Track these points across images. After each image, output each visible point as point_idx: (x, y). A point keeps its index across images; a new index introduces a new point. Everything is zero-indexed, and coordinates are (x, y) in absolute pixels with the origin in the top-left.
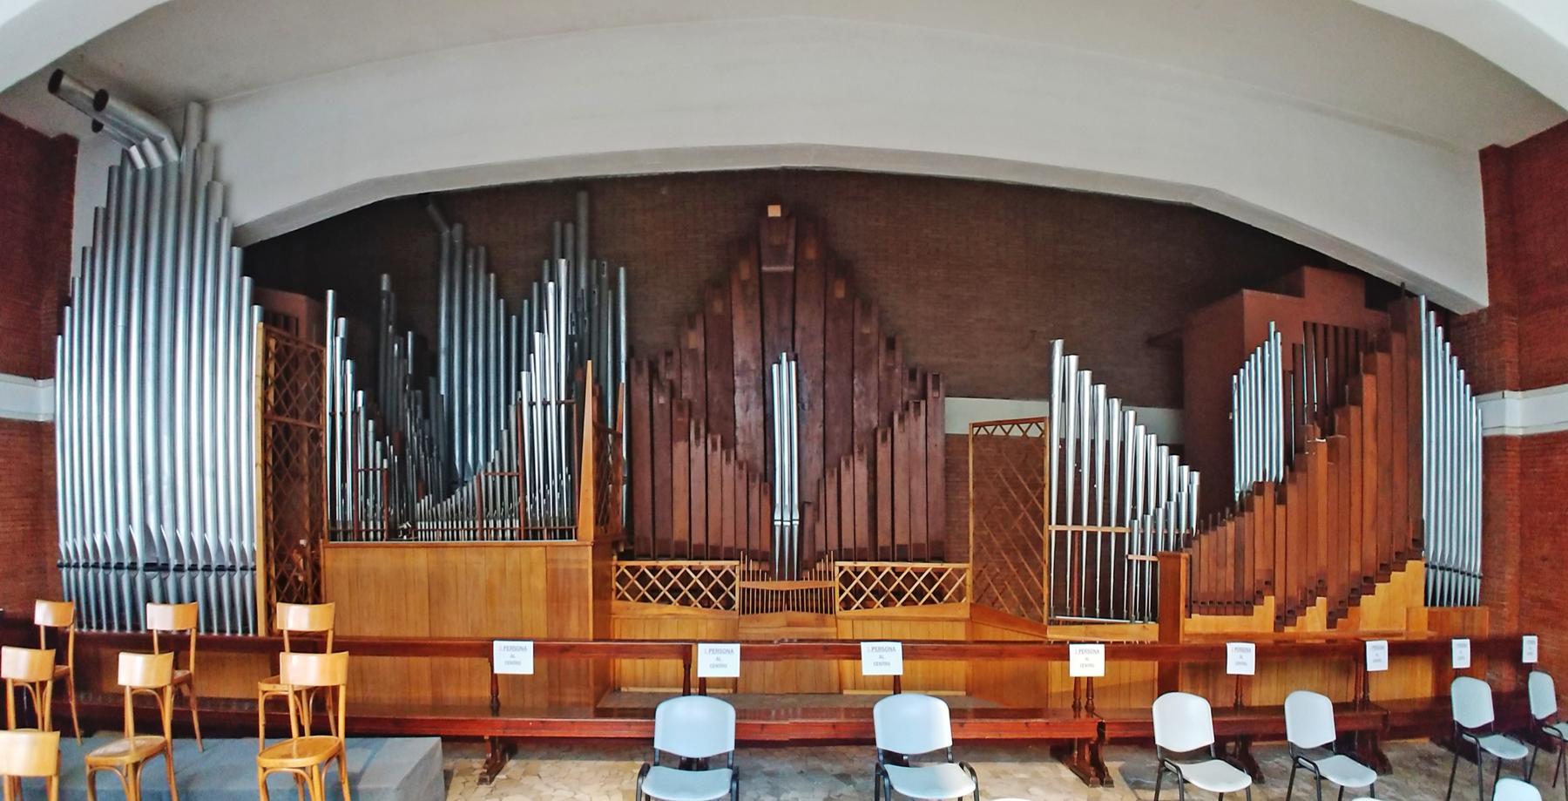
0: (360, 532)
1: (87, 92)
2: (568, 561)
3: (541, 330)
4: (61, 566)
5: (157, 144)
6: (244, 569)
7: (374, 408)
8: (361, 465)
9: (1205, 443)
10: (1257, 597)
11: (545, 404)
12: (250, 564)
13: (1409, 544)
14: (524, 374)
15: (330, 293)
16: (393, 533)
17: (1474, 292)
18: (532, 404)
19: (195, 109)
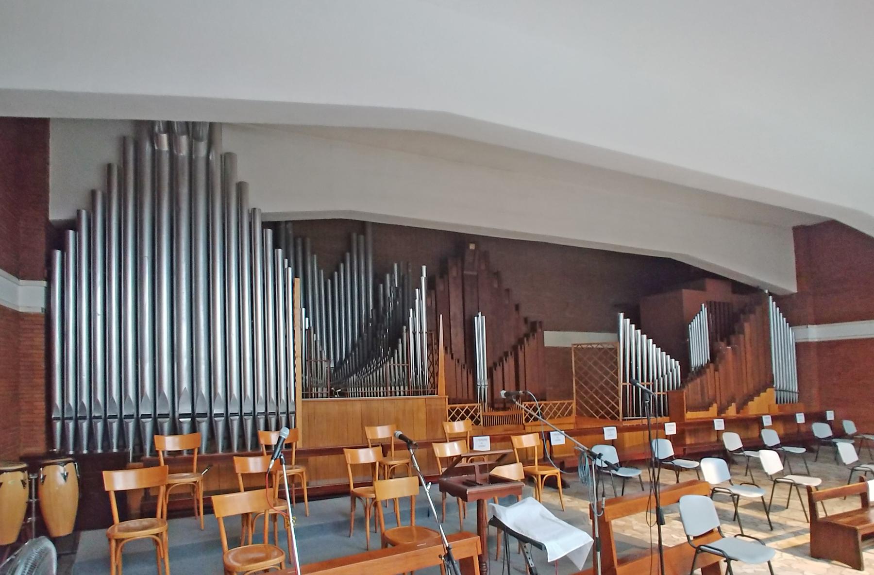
9: (679, 349)
10: (710, 405)
13: (769, 382)
17: (792, 288)
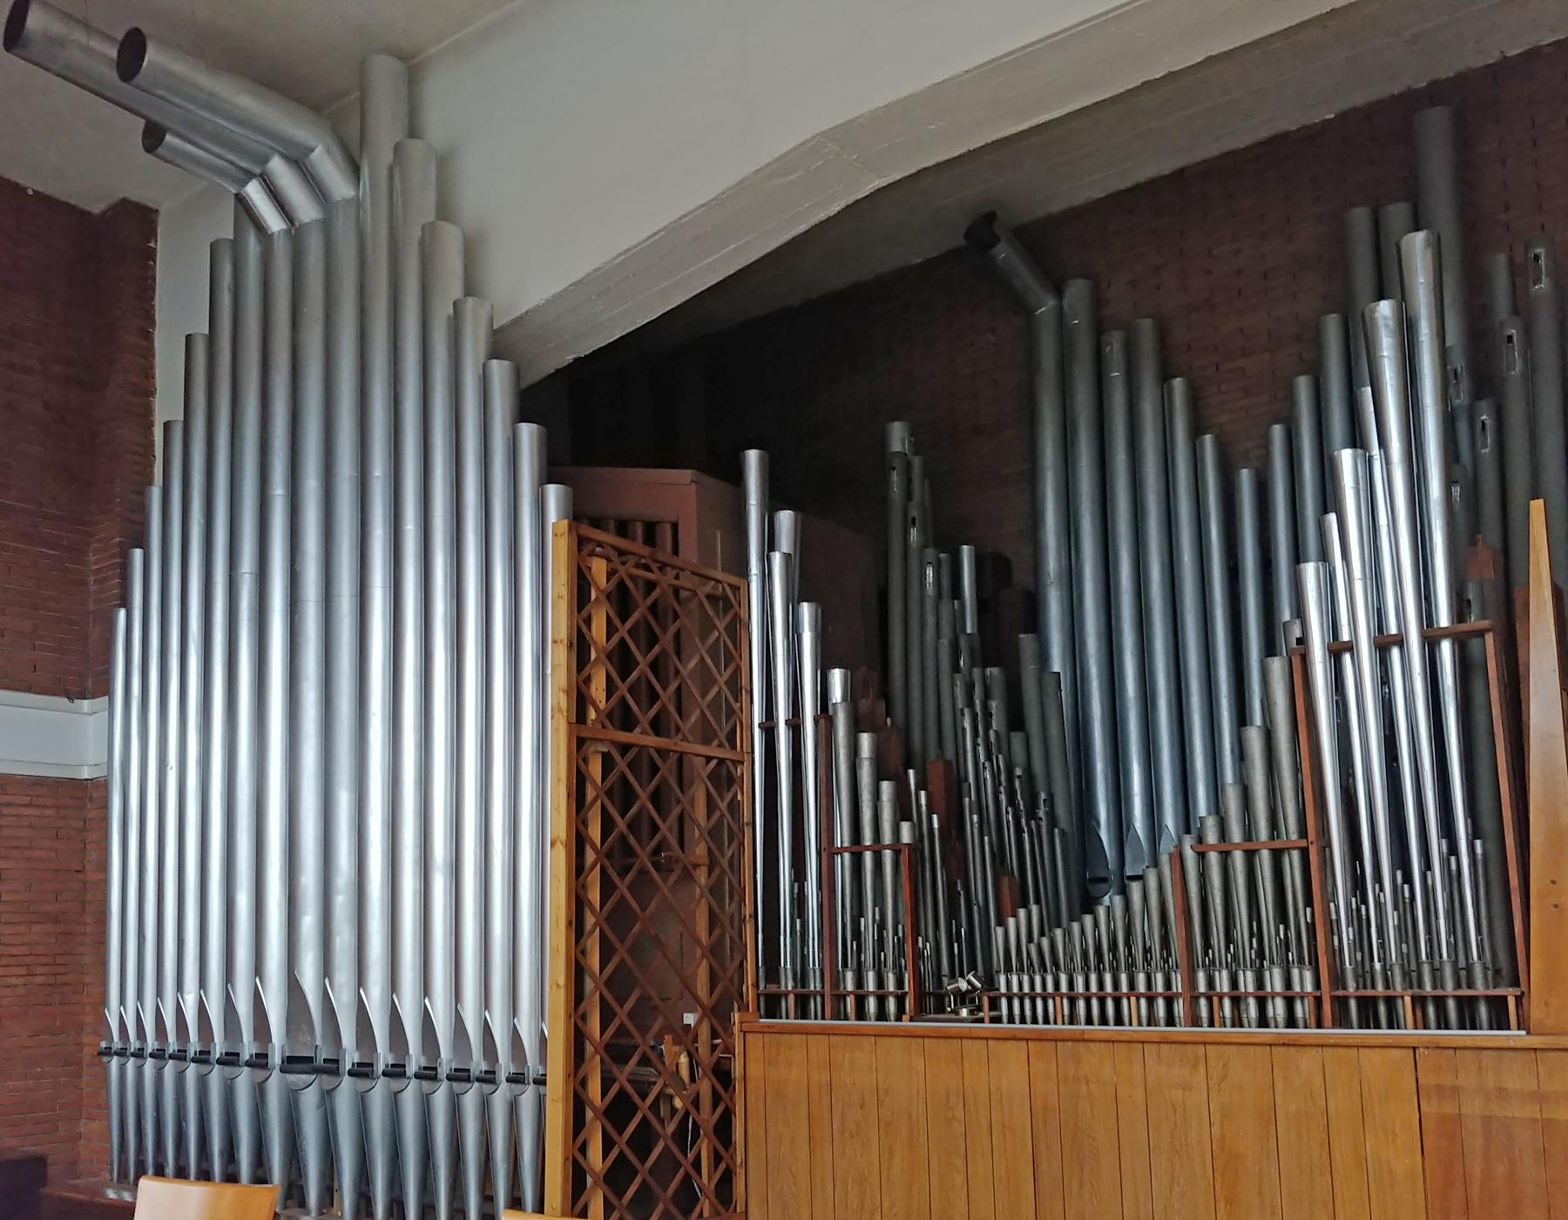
0: (840, 998)
1: (95, 43)
2: (1501, 1092)
3: (1356, 440)
4: (108, 1052)
5: (299, 161)
6: (516, 1079)
7: (876, 700)
8: (842, 836)
11: (1383, 645)
12: (533, 1066)
14: (1310, 570)
15: (753, 457)
16: (931, 1001)
18: (1336, 651)
19: (384, 71)
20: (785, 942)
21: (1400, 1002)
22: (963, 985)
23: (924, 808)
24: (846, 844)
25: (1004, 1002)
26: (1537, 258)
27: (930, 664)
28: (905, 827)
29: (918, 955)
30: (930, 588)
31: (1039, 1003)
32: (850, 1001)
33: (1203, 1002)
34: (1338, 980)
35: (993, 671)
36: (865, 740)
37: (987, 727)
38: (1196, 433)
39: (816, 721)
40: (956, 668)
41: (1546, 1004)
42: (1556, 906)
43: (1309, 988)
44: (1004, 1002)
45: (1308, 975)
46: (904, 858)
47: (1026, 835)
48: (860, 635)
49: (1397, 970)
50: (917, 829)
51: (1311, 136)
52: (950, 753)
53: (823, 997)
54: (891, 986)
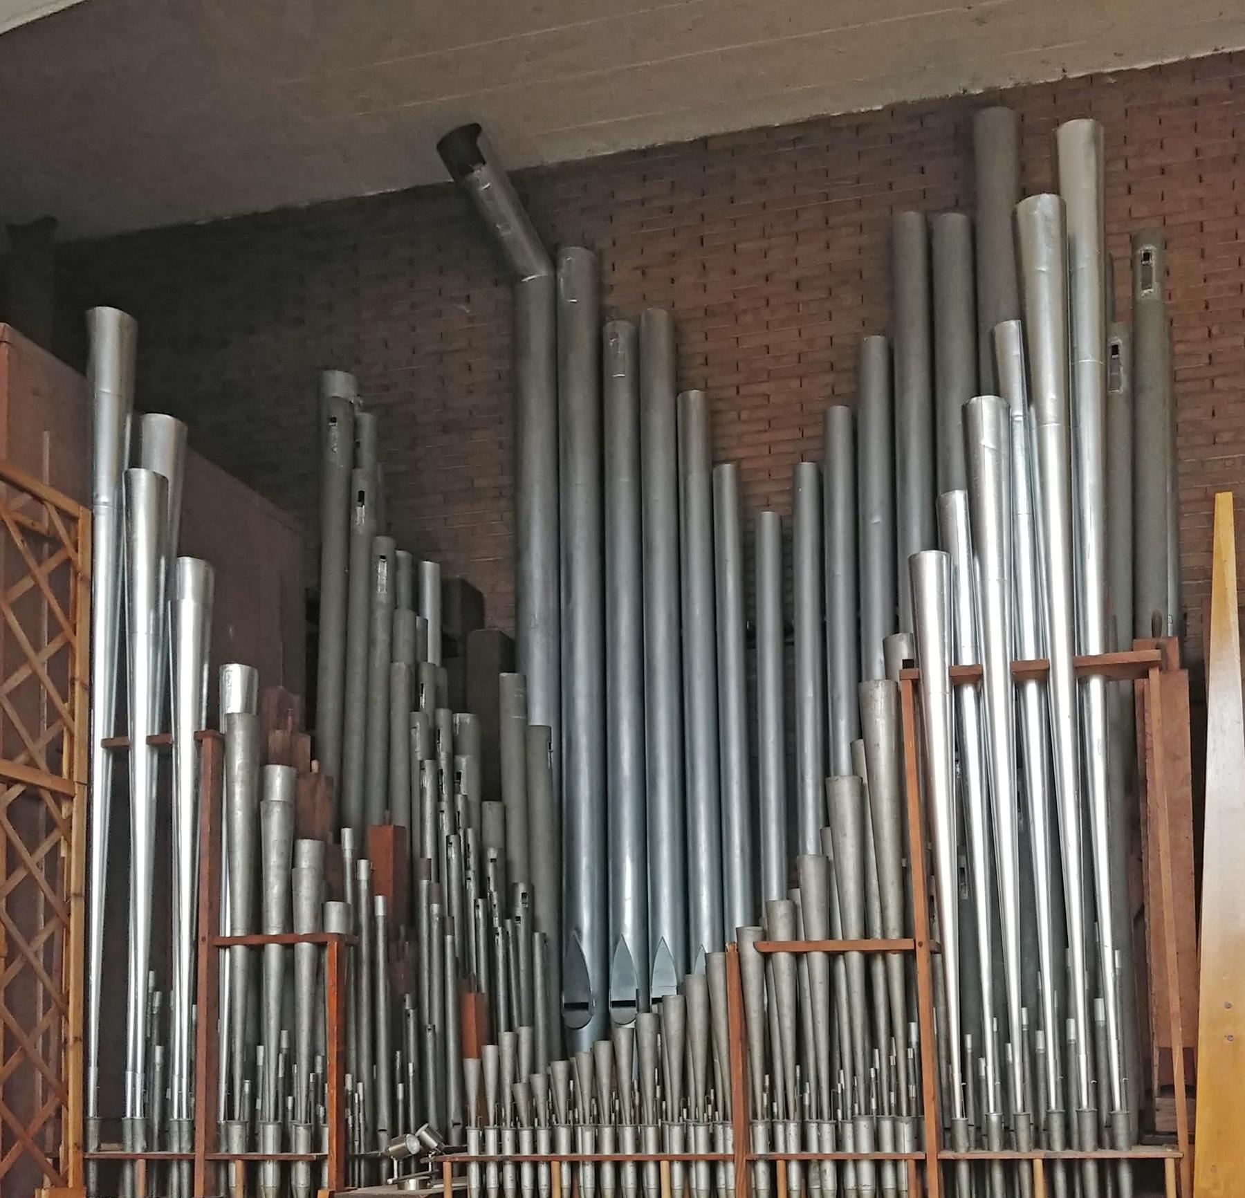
7: (296, 707)
8: (233, 920)
20: (134, 1080)
21: (1025, 1168)
22: (414, 1146)
23: (364, 886)
24: (239, 933)
25: (474, 1169)
26: (1147, 256)
27: (378, 697)
28: (335, 911)
29: (345, 1101)
30: (382, 593)
31: (526, 1170)
32: (236, 1170)
33: (762, 1168)
34: (947, 1134)
35: (465, 719)
36: (278, 777)
37: (454, 791)
38: (713, 462)
39: (198, 740)
40: (415, 706)
41: (1214, 1169)
42: (1230, 1037)
43: (906, 1146)
44: (474, 1169)
45: (906, 1130)
46: (330, 955)
47: (499, 939)
48: (275, 626)
49: (1023, 1124)
50: (352, 913)
51: (858, 125)
52: (401, 820)
53: (192, 1163)
54: (301, 1146)
